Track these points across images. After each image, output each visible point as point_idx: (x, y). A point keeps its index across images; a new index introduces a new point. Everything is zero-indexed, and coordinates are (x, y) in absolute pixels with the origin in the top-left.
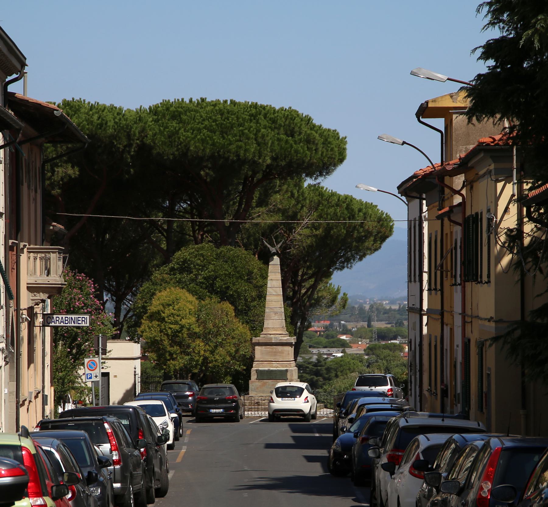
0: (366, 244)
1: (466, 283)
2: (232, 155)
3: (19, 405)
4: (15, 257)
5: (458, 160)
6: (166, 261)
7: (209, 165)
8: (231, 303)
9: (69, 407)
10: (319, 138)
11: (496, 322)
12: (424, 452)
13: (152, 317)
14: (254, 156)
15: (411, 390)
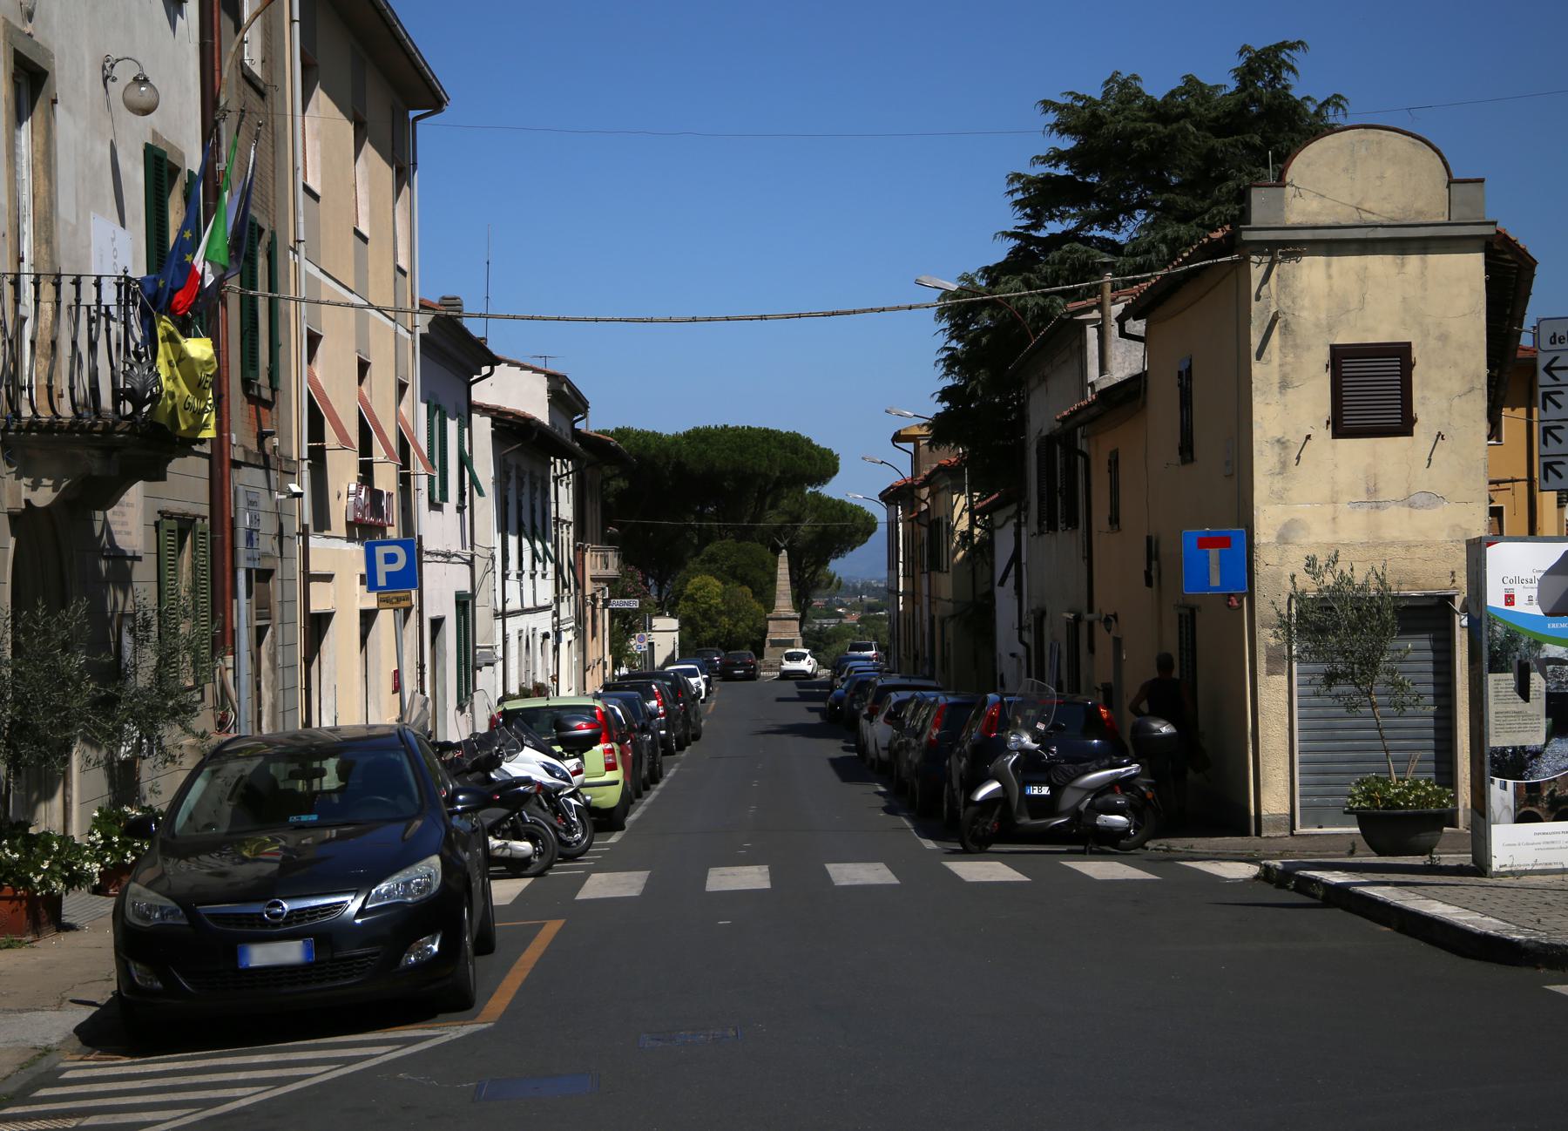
3: (585, 670)
6: (697, 555)
9: (624, 671)
12: (895, 705)
13: (688, 598)
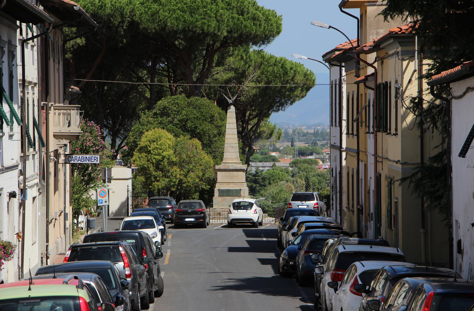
0: (296, 93)
1: (378, 133)
2: (198, 29)
4: (45, 115)
5: (373, 43)
6: (149, 108)
7: (182, 37)
8: (198, 139)
10: (262, 16)
11: (402, 164)
13: (142, 150)
14: (215, 30)
15: (333, 205)
